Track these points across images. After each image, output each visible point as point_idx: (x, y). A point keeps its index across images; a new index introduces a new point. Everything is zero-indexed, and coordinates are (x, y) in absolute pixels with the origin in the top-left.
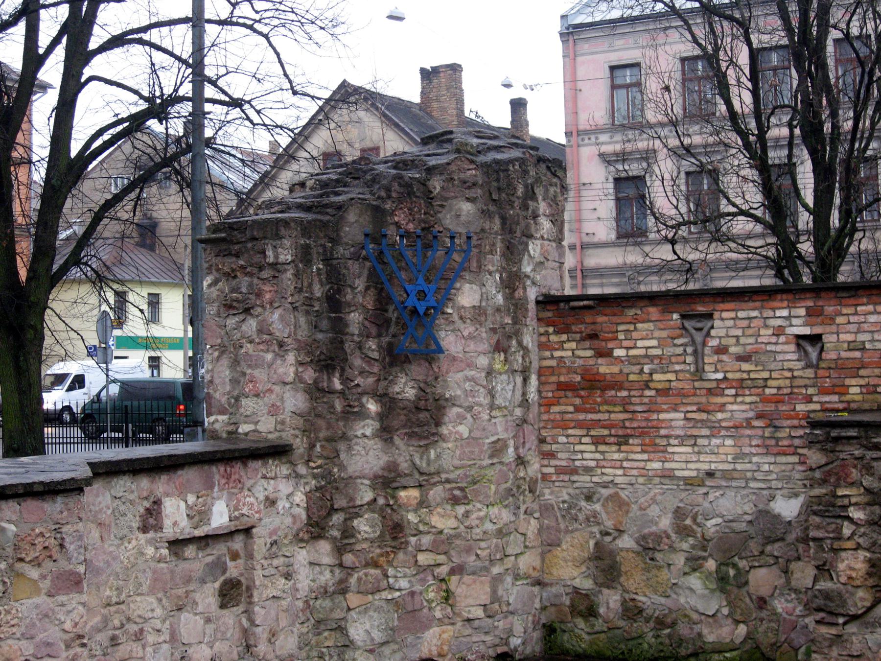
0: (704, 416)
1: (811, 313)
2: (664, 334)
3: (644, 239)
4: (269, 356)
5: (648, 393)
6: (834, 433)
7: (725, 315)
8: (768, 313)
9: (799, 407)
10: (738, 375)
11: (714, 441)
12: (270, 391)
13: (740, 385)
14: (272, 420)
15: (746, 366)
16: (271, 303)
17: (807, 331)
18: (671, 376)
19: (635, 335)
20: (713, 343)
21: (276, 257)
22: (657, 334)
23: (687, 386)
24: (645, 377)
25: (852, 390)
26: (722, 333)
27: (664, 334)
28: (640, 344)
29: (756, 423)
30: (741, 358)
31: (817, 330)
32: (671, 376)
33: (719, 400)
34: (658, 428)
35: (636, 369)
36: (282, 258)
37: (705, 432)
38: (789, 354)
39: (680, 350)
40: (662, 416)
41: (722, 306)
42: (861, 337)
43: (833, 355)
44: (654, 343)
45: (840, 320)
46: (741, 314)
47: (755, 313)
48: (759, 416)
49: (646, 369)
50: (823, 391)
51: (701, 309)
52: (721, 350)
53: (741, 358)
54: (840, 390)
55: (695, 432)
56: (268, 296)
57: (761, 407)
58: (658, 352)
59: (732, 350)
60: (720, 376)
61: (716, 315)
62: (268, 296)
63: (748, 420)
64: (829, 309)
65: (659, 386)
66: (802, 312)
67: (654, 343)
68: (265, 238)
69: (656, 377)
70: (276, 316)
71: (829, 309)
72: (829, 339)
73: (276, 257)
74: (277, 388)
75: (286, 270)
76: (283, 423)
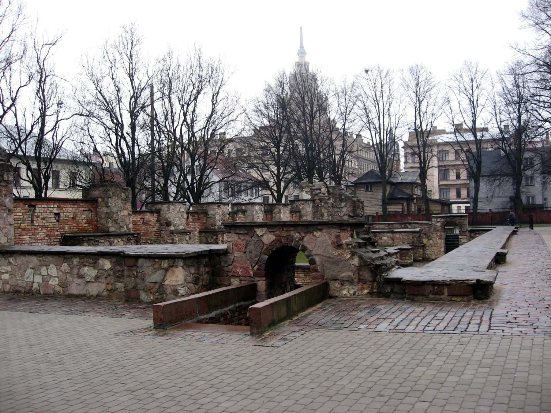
0: (34, 236)
1: (58, 207)
2: (24, 211)
3: (230, 193)
4: (5, 215)
5: (20, 230)
6: (90, 238)
7: (39, 206)
8: (49, 206)
9: (56, 233)
10: (42, 224)
11: (37, 244)
12: (5, 227)
13: (42, 227)
14: (6, 238)
15: (44, 222)
16: (6, 195)
17: (57, 212)
18: (26, 224)
19: (16, 211)
20: (36, 214)
21: (8, 178)
22: (22, 211)
23: (29, 227)
24: (19, 225)
25: (67, 228)
26: (38, 211)
27: (24, 211)
28: (17, 214)
29: (46, 238)
30: (43, 219)
31: (59, 211)
32: (26, 224)
33: (37, 231)
34: (22, 241)
35: (16, 222)
36: (10, 179)
37: (34, 241)
38: (53, 219)
39: (28, 216)
40: (23, 237)
41: (38, 203)
42: (68, 214)
43: (62, 219)
44: (21, 214)
45: (64, 209)
46: (43, 206)
47: (46, 206)
48: (46, 236)
49: (19, 222)
50: (61, 229)
51: (33, 204)
52: (38, 217)
53: (43, 219)
54: (63, 228)
55: (32, 241)
56: (4, 192)
57: (47, 233)
58: (22, 217)
59: (41, 216)
60: (37, 224)
61: (37, 206)
62: (4, 192)
63: (44, 237)
64: (62, 206)
65: (23, 227)
66: (56, 206)
67: (21, 214)
68: (3, 170)
69: (22, 225)
70: (8, 200)
71: (62, 206)
72: (62, 214)
73: (8, 178)
74: (8, 227)
75: (11, 183)
76: (11, 239)
